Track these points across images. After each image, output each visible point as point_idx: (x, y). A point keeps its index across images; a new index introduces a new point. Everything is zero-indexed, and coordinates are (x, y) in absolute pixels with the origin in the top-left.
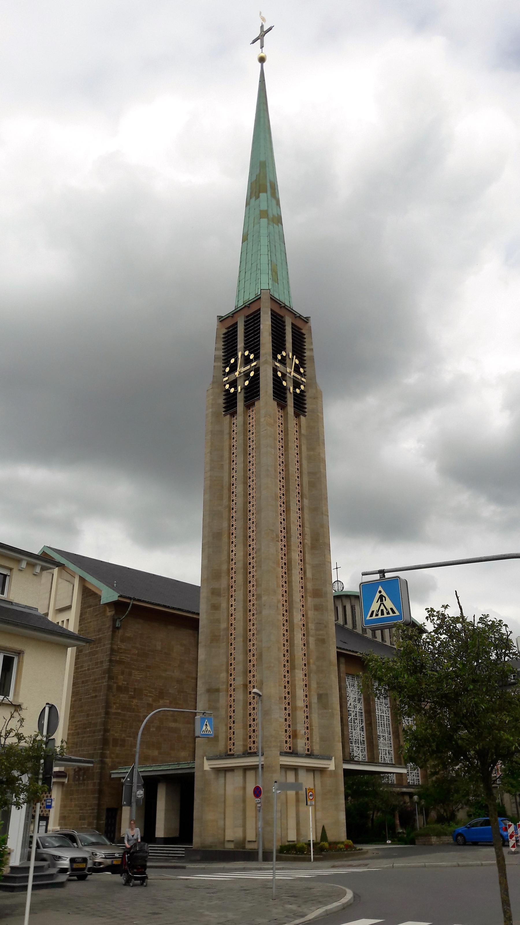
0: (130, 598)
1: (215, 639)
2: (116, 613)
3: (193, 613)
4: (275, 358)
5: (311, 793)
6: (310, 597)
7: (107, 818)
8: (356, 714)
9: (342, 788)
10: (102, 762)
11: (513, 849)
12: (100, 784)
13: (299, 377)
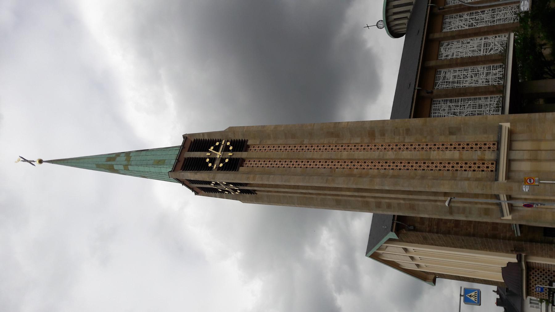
0: (393, 223)
1: (412, 208)
3: (393, 220)
4: (211, 169)
5: (528, 181)
8: (472, 19)
9: (526, 115)
10: (509, 239)
13: (222, 146)
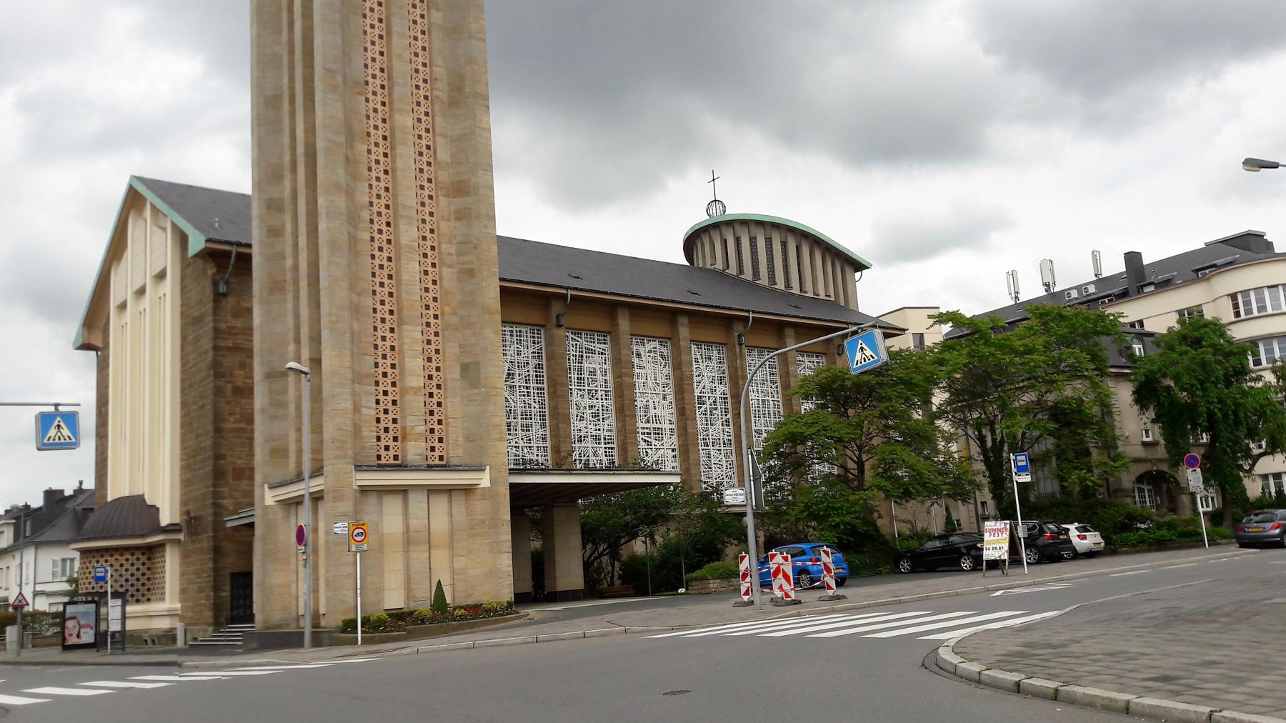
1: (276, 287)
2: (219, 271)
6: (445, 196)
7: (232, 588)
10: (216, 505)
11: (746, 598)
12: (215, 537)
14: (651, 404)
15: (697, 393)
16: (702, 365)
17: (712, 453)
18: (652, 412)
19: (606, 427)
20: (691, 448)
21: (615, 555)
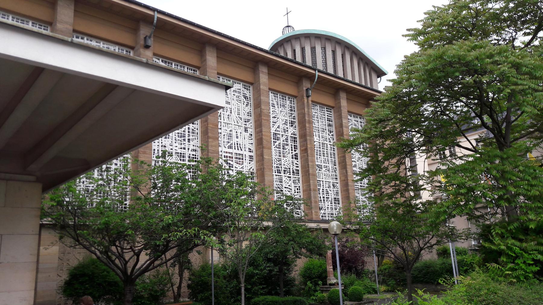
14: (234, 134)
15: (273, 130)
16: (278, 110)
17: (284, 179)
18: (235, 140)
19: (191, 147)
20: (267, 172)
21: (183, 263)
